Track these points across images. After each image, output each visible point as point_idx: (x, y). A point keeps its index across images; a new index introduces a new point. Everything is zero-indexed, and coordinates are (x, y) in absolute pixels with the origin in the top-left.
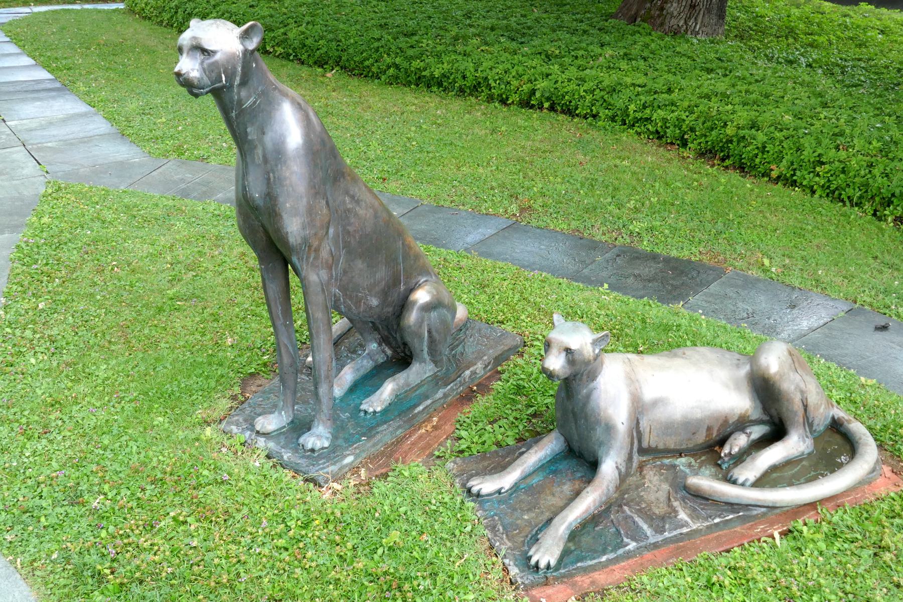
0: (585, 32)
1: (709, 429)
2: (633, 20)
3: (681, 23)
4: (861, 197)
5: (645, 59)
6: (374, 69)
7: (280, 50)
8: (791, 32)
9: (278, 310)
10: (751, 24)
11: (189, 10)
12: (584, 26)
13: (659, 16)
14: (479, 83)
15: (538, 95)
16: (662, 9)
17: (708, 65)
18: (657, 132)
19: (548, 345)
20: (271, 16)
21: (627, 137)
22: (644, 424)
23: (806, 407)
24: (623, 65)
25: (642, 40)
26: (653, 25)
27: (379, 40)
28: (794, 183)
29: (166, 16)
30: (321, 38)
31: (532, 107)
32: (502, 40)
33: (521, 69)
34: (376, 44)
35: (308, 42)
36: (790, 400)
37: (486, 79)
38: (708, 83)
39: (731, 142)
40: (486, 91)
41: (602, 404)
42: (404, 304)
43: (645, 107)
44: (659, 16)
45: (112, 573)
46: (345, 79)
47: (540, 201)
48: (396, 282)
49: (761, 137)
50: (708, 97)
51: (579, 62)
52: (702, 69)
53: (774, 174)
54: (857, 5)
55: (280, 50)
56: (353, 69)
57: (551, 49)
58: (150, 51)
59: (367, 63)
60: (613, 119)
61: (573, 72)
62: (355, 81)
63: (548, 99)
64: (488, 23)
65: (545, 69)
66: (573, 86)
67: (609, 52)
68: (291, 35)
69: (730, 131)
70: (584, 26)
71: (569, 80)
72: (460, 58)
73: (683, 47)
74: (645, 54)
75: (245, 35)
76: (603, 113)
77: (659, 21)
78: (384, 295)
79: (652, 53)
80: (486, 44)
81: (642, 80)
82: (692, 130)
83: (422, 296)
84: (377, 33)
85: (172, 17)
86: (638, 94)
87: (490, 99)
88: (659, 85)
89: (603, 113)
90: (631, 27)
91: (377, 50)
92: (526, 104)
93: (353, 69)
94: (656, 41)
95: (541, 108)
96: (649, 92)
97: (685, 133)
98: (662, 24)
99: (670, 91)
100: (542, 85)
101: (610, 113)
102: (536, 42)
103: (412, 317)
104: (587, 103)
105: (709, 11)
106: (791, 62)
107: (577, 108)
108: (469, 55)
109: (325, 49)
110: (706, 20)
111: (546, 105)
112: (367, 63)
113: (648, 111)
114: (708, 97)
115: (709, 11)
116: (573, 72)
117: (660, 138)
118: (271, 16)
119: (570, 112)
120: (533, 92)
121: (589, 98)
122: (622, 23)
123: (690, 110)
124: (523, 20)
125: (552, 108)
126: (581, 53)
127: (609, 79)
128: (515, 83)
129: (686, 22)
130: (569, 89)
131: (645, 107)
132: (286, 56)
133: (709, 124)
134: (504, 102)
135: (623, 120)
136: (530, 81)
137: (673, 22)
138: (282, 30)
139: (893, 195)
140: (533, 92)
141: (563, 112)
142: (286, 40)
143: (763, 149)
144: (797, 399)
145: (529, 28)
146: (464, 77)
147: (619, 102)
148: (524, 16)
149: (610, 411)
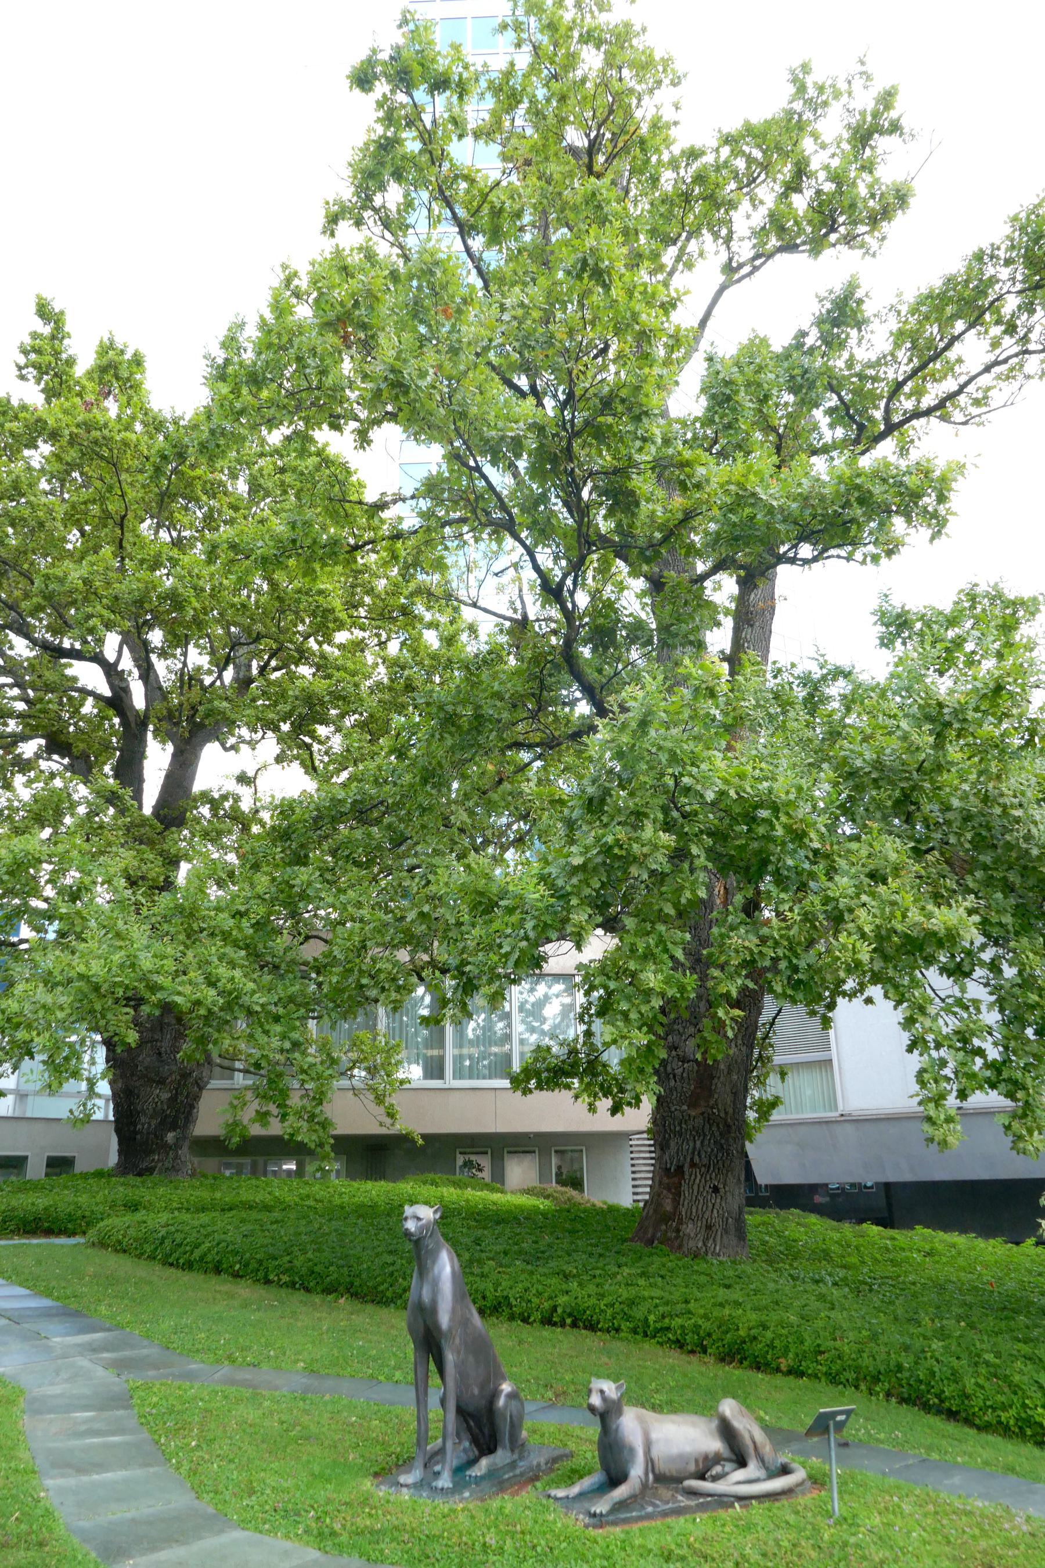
0: (601, 1255)
1: (697, 1461)
2: (650, 1242)
3: (700, 1244)
4: (857, 1379)
5: (662, 1277)
6: (389, 1294)
7: (285, 1278)
8: (826, 1255)
9: (421, 1389)
10: (782, 1248)
11: (178, 1241)
12: (599, 1250)
13: (677, 1238)
14: (500, 1303)
15: (560, 1310)
16: (678, 1231)
17: (727, 1282)
18: (678, 1341)
19: (590, 1391)
20: (272, 1245)
21: (648, 1345)
22: (655, 1453)
23: (754, 1443)
24: (642, 1282)
25: (657, 1261)
26: (672, 1248)
27: (393, 1264)
28: (802, 1374)
29: (148, 1248)
30: (332, 1264)
31: (555, 1324)
32: (518, 1263)
33: (540, 1287)
34: (391, 1269)
35: (317, 1269)
36: (743, 1437)
37: (507, 1298)
38: (722, 1294)
39: (744, 1342)
40: (507, 1311)
41: (626, 1434)
42: (495, 1394)
43: (663, 1317)
44: (677, 1238)
45: (676, 1048)
46: (357, 1305)
47: (572, 1388)
48: (487, 1380)
49: (769, 1335)
50: (722, 1305)
51: (598, 1280)
52: (720, 1285)
53: (784, 1367)
54: (913, 1229)
55: (285, 1278)
56: (366, 1295)
57: (569, 1268)
58: (150, 1283)
59: (381, 1288)
60: (634, 1331)
61: (591, 1289)
62: (370, 1307)
63: (570, 1315)
64: (498, 1248)
65: (564, 1287)
66: (593, 1301)
67: (626, 1271)
68: (297, 1263)
69: (742, 1333)
70: (599, 1250)
71: (589, 1296)
72: (478, 1279)
73: (702, 1266)
74: (662, 1273)
75: (435, 1212)
76: (625, 1325)
77: (676, 1244)
78: (482, 1388)
79: (671, 1271)
80: (501, 1266)
81: (658, 1293)
82: (709, 1335)
83: (506, 1387)
84: (389, 1259)
85: (156, 1249)
86: (656, 1306)
87: (512, 1318)
88: (676, 1296)
89: (625, 1325)
90: (647, 1250)
91: (392, 1274)
92: (548, 1321)
93: (366, 1295)
94: (672, 1261)
95: (563, 1325)
96: (667, 1303)
97: (703, 1339)
98: (680, 1247)
99: (687, 1302)
100: (562, 1300)
101: (631, 1326)
102: (552, 1264)
103: (501, 1402)
104: (608, 1317)
105: (726, 1231)
106: (817, 1282)
107: (598, 1322)
108: (487, 1276)
109: (335, 1276)
110: (725, 1241)
111: (569, 1321)
112: (381, 1288)
113: (667, 1320)
114: (722, 1305)
115: (726, 1231)
116: (591, 1289)
117: (681, 1347)
118: (272, 1245)
119: (592, 1327)
120: (554, 1309)
121: (609, 1311)
122: (638, 1246)
123: (706, 1317)
124: (535, 1246)
125: (574, 1325)
126: (598, 1272)
127: (625, 1293)
128: (535, 1300)
129: (704, 1244)
130: (590, 1303)
131: (663, 1317)
132: (292, 1285)
133: (724, 1328)
134: (525, 1320)
135: (644, 1331)
136: (550, 1298)
137: (691, 1244)
138: (288, 1258)
139: (879, 1373)
140: (554, 1309)
141: (585, 1328)
142: (292, 1268)
143: (771, 1346)
144: (748, 1441)
145: (543, 1252)
146: (484, 1298)
147: (639, 1313)
148: (536, 1242)
149: (631, 1438)
